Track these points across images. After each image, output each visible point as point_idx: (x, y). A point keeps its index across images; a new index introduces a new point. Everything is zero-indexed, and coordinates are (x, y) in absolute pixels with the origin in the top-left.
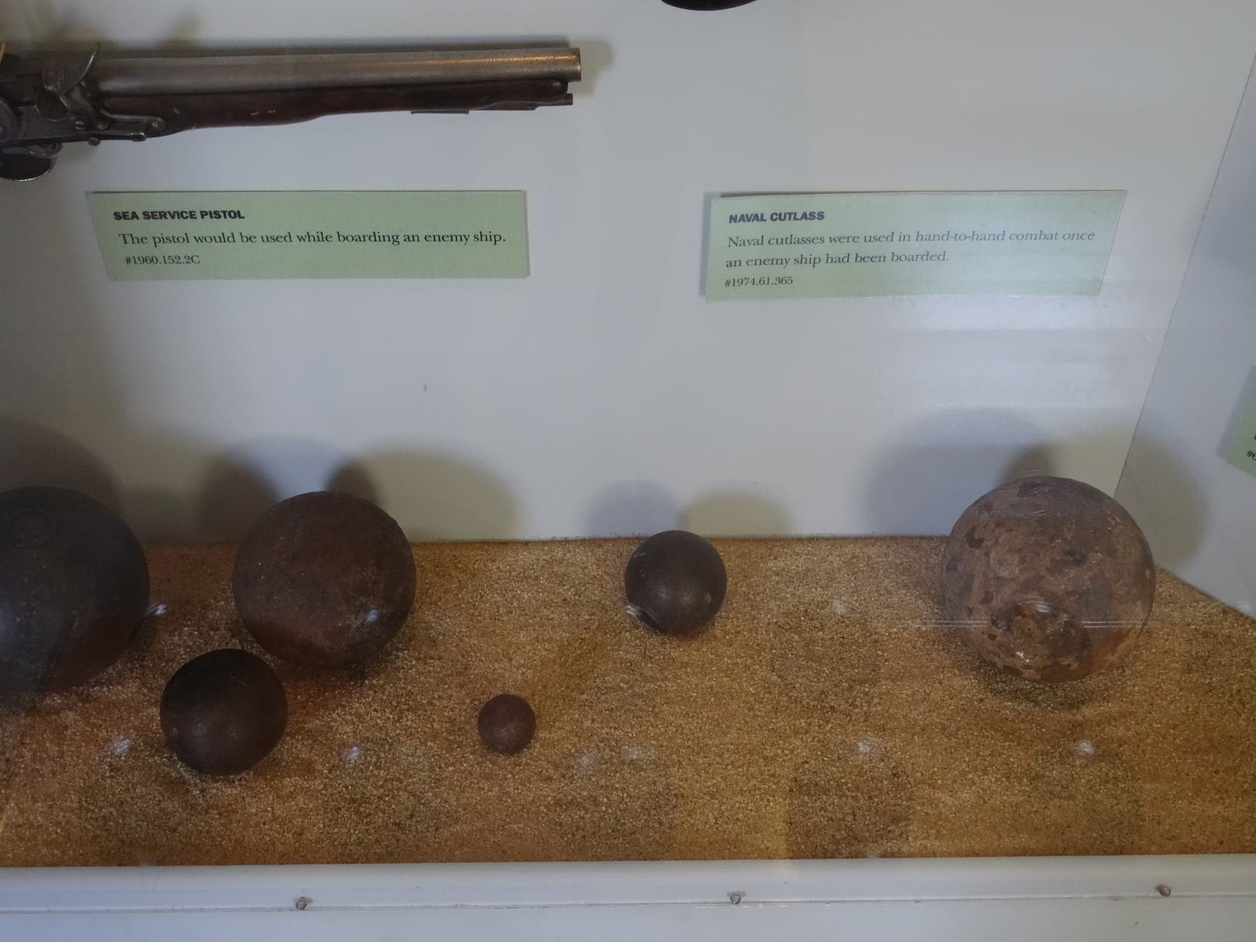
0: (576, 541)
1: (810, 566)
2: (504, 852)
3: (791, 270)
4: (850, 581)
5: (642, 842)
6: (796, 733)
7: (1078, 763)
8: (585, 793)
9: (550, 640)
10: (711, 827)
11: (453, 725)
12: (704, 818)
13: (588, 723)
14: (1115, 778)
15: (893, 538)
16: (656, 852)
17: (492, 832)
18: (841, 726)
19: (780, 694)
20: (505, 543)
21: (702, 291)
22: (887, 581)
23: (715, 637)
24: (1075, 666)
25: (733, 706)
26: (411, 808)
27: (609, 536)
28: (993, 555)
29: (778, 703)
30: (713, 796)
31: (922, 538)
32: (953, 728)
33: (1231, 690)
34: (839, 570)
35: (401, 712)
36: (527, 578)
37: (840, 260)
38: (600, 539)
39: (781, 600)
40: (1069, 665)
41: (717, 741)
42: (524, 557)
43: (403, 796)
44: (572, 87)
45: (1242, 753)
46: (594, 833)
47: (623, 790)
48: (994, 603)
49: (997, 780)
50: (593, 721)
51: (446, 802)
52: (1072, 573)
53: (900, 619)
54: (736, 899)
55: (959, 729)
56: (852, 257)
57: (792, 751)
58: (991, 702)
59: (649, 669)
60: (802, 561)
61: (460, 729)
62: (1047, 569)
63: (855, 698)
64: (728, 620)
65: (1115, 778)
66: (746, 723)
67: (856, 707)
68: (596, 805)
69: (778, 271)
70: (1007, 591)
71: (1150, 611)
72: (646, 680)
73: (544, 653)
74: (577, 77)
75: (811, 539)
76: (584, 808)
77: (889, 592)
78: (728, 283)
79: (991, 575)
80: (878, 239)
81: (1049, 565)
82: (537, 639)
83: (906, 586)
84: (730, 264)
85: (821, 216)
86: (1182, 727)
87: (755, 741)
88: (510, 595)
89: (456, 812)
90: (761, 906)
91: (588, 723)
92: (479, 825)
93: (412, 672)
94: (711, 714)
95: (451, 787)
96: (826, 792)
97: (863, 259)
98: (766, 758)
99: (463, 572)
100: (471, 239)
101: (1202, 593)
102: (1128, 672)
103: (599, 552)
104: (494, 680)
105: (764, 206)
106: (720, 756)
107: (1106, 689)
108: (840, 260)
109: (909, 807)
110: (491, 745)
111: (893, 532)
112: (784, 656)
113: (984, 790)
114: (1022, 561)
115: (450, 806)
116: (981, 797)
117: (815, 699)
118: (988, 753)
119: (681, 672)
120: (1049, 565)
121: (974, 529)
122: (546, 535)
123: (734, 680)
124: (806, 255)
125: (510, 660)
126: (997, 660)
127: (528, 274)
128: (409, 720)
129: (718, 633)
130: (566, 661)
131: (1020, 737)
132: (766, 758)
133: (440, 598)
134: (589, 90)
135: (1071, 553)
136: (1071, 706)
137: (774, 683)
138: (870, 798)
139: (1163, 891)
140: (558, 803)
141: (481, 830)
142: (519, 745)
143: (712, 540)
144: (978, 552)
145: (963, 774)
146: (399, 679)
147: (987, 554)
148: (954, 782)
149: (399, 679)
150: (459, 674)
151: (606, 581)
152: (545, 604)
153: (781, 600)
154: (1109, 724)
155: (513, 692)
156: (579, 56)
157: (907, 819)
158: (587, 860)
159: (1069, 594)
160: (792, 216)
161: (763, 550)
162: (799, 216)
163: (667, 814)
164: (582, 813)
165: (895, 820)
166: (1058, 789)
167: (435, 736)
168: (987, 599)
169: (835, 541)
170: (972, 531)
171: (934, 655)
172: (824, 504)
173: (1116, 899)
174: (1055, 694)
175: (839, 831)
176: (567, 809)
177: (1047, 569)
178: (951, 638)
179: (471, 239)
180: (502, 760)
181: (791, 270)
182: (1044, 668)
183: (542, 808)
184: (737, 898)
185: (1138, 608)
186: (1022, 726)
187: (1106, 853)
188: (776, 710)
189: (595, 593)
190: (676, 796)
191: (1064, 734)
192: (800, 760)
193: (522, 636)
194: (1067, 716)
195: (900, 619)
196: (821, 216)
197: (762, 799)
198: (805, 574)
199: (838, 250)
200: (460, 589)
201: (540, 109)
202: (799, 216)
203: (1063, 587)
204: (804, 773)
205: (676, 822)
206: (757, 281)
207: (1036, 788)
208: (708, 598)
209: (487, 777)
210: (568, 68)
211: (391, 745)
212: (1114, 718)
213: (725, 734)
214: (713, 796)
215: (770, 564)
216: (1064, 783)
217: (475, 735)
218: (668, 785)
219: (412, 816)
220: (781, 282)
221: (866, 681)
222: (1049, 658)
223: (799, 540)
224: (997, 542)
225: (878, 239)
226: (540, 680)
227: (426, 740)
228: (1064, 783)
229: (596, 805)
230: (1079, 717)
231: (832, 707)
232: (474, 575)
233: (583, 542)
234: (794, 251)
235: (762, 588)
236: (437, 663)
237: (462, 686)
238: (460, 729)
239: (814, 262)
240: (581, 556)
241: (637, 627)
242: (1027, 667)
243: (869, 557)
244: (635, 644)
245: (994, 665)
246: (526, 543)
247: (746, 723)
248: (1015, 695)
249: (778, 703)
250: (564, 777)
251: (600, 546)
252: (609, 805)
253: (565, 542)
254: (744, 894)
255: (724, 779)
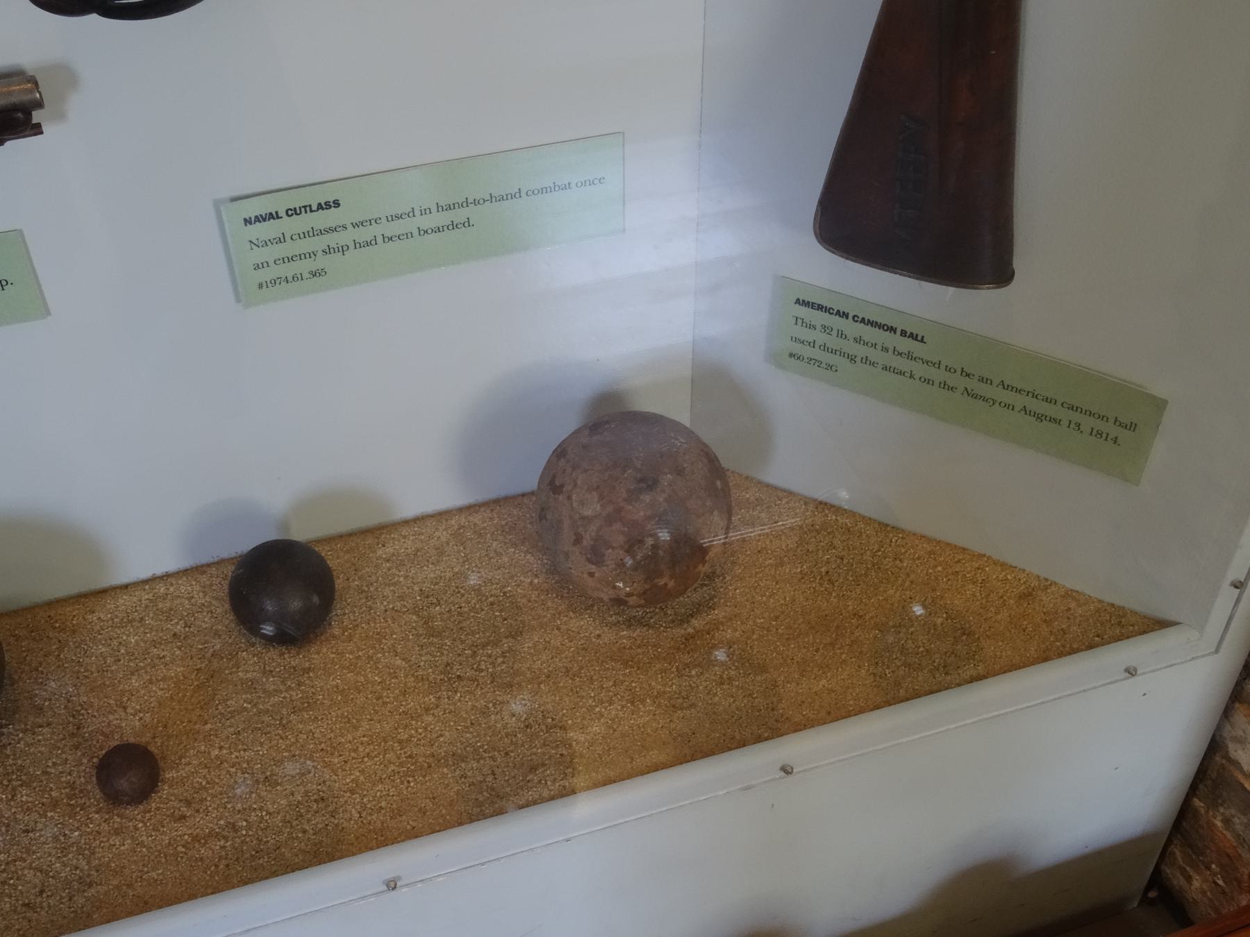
0: (178, 573)
1: (419, 545)
2: (146, 903)
3: (321, 262)
4: (459, 552)
5: (288, 855)
6: (427, 710)
7: (693, 672)
8: (222, 822)
9: (164, 679)
10: (356, 822)
11: (73, 789)
12: (347, 816)
13: (217, 752)
14: (729, 678)
15: (497, 501)
16: (303, 861)
17: (129, 886)
18: (470, 692)
19: (406, 676)
20: (103, 592)
21: (238, 300)
22: (495, 544)
23: (334, 637)
24: (671, 584)
25: (360, 699)
26: (39, 885)
27: (211, 560)
28: (574, 497)
29: (405, 684)
30: (352, 792)
31: (523, 495)
32: (576, 669)
33: (820, 573)
34: (448, 543)
35: (14, 789)
36: (130, 622)
37: (368, 244)
38: (202, 566)
39: (395, 584)
40: (666, 584)
41: (350, 737)
42: (124, 600)
43: (29, 874)
44: (37, 116)
45: (838, 627)
46: (237, 859)
47: (261, 809)
48: (585, 543)
49: (623, 707)
50: (221, 748)
51: (76, 868)
52: (647, 498)
53: (512, 577)
54: (392, 885)
55: (582, 668)
56: (380, 239)
57: (426, 728)
58: (608, 636)
59: (271, 683)
60: (410, 543)
61: (81, 791)
62: (625, 500)
63: (479, 662)
64: (345, 614)
65: (729, 678)
66: (376, 712)
67: (482, 671)
68: (236, 831)
69: (305, 266)
70: (593, 528)
71: (729, 519)
72: (269, 694)
73: (160, 693)
74: (39, 104)
75: (418, 520)
76: (224, 837)
77: (499, 554)
78: (260, 286)
79: (577, 517)
80: (399, 217)
81: (625, 495)
82: (151, 682)
83: (514, 545)
84: (257, 267)
85: (337, 204)
86: (782, 617)
87: (387, 727)
88: (116, 642)
89: (89, 875)
90: (420, 885)
91: (217, 752)
92: (115, 882)
93: (22, 745)
94: (339, 712)
95: (80, 852)
96: (464, 759)
97: (390, 239)
98: (400, 742)
99: (62, 630)
100: (320, 253)
101: (784, 491)
102: (728, 578)
103: (204, 579)
104: (112, 732)
105: (279, 204)
106: (355, 751)
107: (711, 599)
108: (368, 244)
109: (544, 754)
110: (115, 799)
111: (503, 493)
112: (406, 639)
113: (613, 720)
114: (601, 497)
115: (82, 871)
116: (610, 727)
117: (442, 673)
118: (611, 683)
119: (304, 679)
120: (625, 495)
121: (554, 477)
122: (145, 574)
123: (359, 673)
124: (333, 245)
125: (125, 708)
126: (602, 595)
127: (48, 313)
128: (24, 795)
129: (336, 632)
130: (184, 696)
131: (639, 662)
132: (400, 742)
133: (41, 664)
134: (60, 116)
135: (642, 480)
136: (682, 622)
137: (399, 668)
138: (507, 754)
139: (787, 770)
140: (196, 838)
141: (118, 887)
142: (143, 794)
143: (318, 541)
144: (561, 497)
145: (590, 709)
146: (8, 756)
147: (569, 498)
148: (584, 718)
149: (8, 756)
150: (73, 735)
151: (211, 608)
152: (155, 644)
153: (395, 584)
154: (718, 629)
155: (132, 740)
156: (36, 84)
157: (543, 765)
158: (233, 887)
159: (649, 518)
160: (307, 208)
161: (370, 541)
162: (314, 208)
163: (309, 820)
164: (222, 842)
165: (533, 769)
166: (680, 701)
167: (55, 804)
168: (578, 540)
169: (441, 516)
170: (552, 482)
171: (549, 604)
172: (422, 485)
173: (747, 788)
174: (666, 614)
175: (481, 793)
176: (206, 843)
177: (625, 500)
178: (562, 584)
179: (320, 253)
180: (130, 811)
181: (321, 262)
182: (645, 593)
183: (180, 849)
184: (392, 885)
185: (717, 519)
186: (639, 651)
187: (730, 749)
188: (404, 693)
189: (205, 621)
190: (316, 801)
191: (679, 649)
192: (434, 735)
193: (135, 682)
194: (679, 631)
195: (512, 577)
196: (337, 204)
197: (402, 783)
198: (415, 555)
199: (364, 234)
200: (61, 650)
201: (8, 144)
202: (314, 208)
203: (642, 513)
204: (440, 747)
205: (320, 826)
206: (290, 279)
207: (659, 705)
208: (316, 599)
209: (117, 832)
210: (26, 98)
211: (8, 826)
212: (722, 623)
213: (356, 728)
214: (352, 792)
215: (380, 552)
216: (684, 694)
217: (98, 793)
218: (306, 792)
219: (42, 892)
220: (314, 275)
221: (487, 644)
222: (645, 582)
223: (406, 522)
224: (576, 485)
225: (399, 217)
226: (159, 722)
227: (45, 812)
228: (684, 694)
229: (236, 831)
230: (690, 630)
231: (459, 677)
232: (74, 632)
233: (185, 572)
234: (318, 243)
235: (374, 578)
236: (46, 730)
237: (77, 747)
238: (81, 791)
239: (343, 250)
240: (184, 587)
241: (253, 645)
242: (629, 595)
243: (475, 524)
244: (255, 663)
245: (601, 600)
246: (125, 587)
247: (376, 712)
248: (629, 623)
249: (405, 684)
250: (198, 811)
251: (204, 572)
252: (249, 827)
253: (166, 577)
254: (399, 878)
255: (362, 772)
